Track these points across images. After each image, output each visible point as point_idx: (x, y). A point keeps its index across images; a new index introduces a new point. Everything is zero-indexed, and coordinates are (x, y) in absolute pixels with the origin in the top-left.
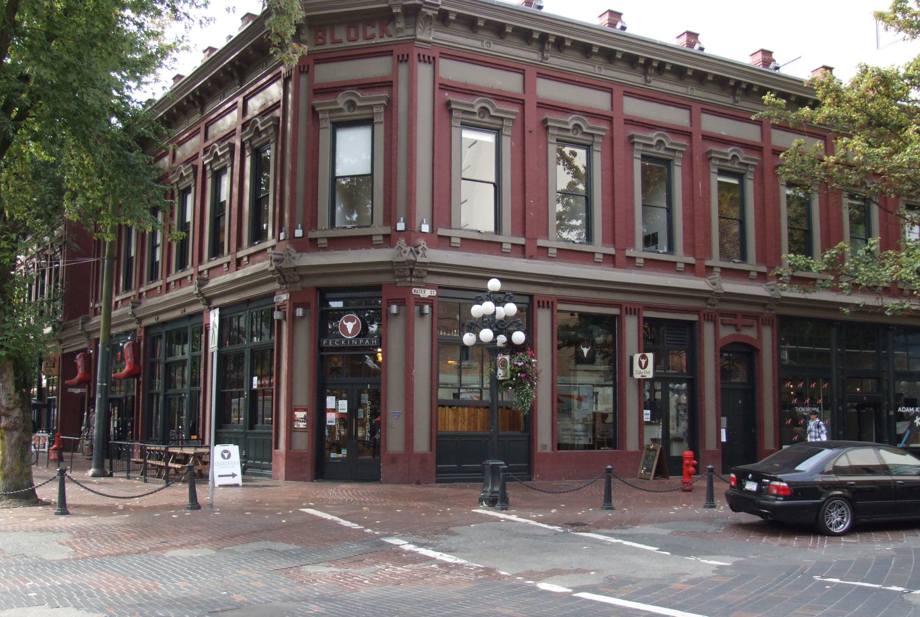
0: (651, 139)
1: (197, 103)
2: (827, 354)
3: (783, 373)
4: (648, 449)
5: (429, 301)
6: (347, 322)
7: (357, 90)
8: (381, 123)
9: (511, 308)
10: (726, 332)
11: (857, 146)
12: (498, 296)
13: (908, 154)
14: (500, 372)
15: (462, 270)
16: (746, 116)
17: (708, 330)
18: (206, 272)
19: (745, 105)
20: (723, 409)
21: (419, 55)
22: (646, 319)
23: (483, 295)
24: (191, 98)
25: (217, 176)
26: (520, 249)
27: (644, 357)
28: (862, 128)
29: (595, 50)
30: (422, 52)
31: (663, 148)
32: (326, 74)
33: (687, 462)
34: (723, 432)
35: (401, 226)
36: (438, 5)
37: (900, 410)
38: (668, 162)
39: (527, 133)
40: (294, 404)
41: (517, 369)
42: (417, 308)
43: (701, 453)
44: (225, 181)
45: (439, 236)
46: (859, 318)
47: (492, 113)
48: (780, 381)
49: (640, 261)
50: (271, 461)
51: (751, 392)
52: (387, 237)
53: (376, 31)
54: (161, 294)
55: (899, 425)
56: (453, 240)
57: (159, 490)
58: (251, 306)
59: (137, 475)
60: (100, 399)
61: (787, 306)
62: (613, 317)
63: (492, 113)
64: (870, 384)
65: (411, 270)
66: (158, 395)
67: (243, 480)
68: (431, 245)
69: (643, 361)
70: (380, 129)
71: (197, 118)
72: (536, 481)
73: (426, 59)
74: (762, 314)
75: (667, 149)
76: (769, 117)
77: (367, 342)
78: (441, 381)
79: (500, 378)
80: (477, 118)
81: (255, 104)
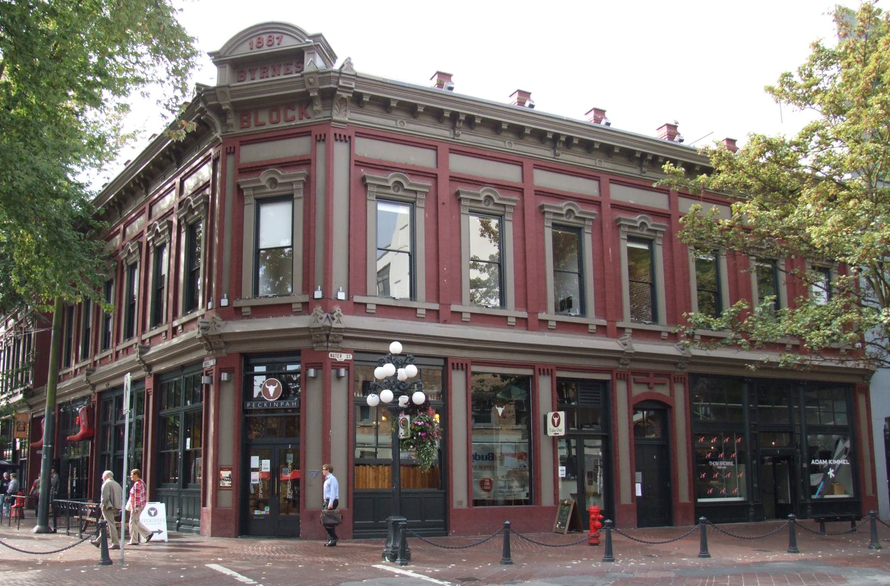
0: (561, 209)
1: (142, 185)
2: (740, 411)
3: (697, 428)
4: (563, 504)
5: (346, 365)
6: (269, 385)
7: (278, 168)
8: (300, 198)
9: (411, 370)
10: (639, 390)
11: (749, 210)
12: (399, 358)
13: (797, 216)
14: (402, 431)
15: (376, 335)
16: (648, 184)
17: (621, 388)
18: (148, 341)
19: (650, 174)
20: (637, 465)
21: (335, 135)
22: (559, 379)
23: (385, 357)
24: (137, 181)
25: (159, 251)
26: (434, 314)
27: (556, 415)
28: (757, 193)
29: (527, 131)
30: (338, 132)
31: (573, 216)
32: (251, 154)
33: (593, 516)
34: (638, 487)
35: (318, 294)
36: (352, 89)
37: (813, 462)
38: (579, 230)
39: (441, 205)
40: (219, 464)
41: (417, 428)
42: (333, 372)
43: (616, 507)
44: (165, 255)
45: (355, 303)
46: (762, 374)
47: (406, 187)
48: (693, 436)
49: (552, 324)
50: (199, 517)
51: (665, 448)
52: (305, 305)
53: (295, 113)
54: (111, 362)
55: (812, 477)
56: (369, 307)
57: (73, 546)
58: (185, 371)
59: (77, 532)
60: (45, 460)
61: (824, 373)
62: (528, 377)
63: (406, 187)
64: (785, 440)
65: (328, 336)
66: (109, 456)
67: (169, 536)
68: (346, 312)
69: (556, 420)
70: (300, 203)
71: (142, 199)
72: (451, 537)
73: (343, 138)
74: (674, 372)
75: (576, 218)
76: (670, 185)
77: (288, 404)
78: (357, 441)
79: (402, 437)
80: (391, 191)
81: (190, 184)
